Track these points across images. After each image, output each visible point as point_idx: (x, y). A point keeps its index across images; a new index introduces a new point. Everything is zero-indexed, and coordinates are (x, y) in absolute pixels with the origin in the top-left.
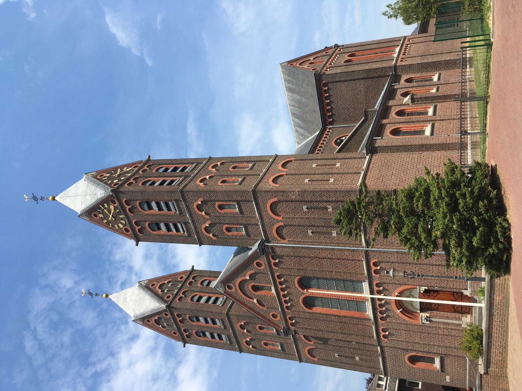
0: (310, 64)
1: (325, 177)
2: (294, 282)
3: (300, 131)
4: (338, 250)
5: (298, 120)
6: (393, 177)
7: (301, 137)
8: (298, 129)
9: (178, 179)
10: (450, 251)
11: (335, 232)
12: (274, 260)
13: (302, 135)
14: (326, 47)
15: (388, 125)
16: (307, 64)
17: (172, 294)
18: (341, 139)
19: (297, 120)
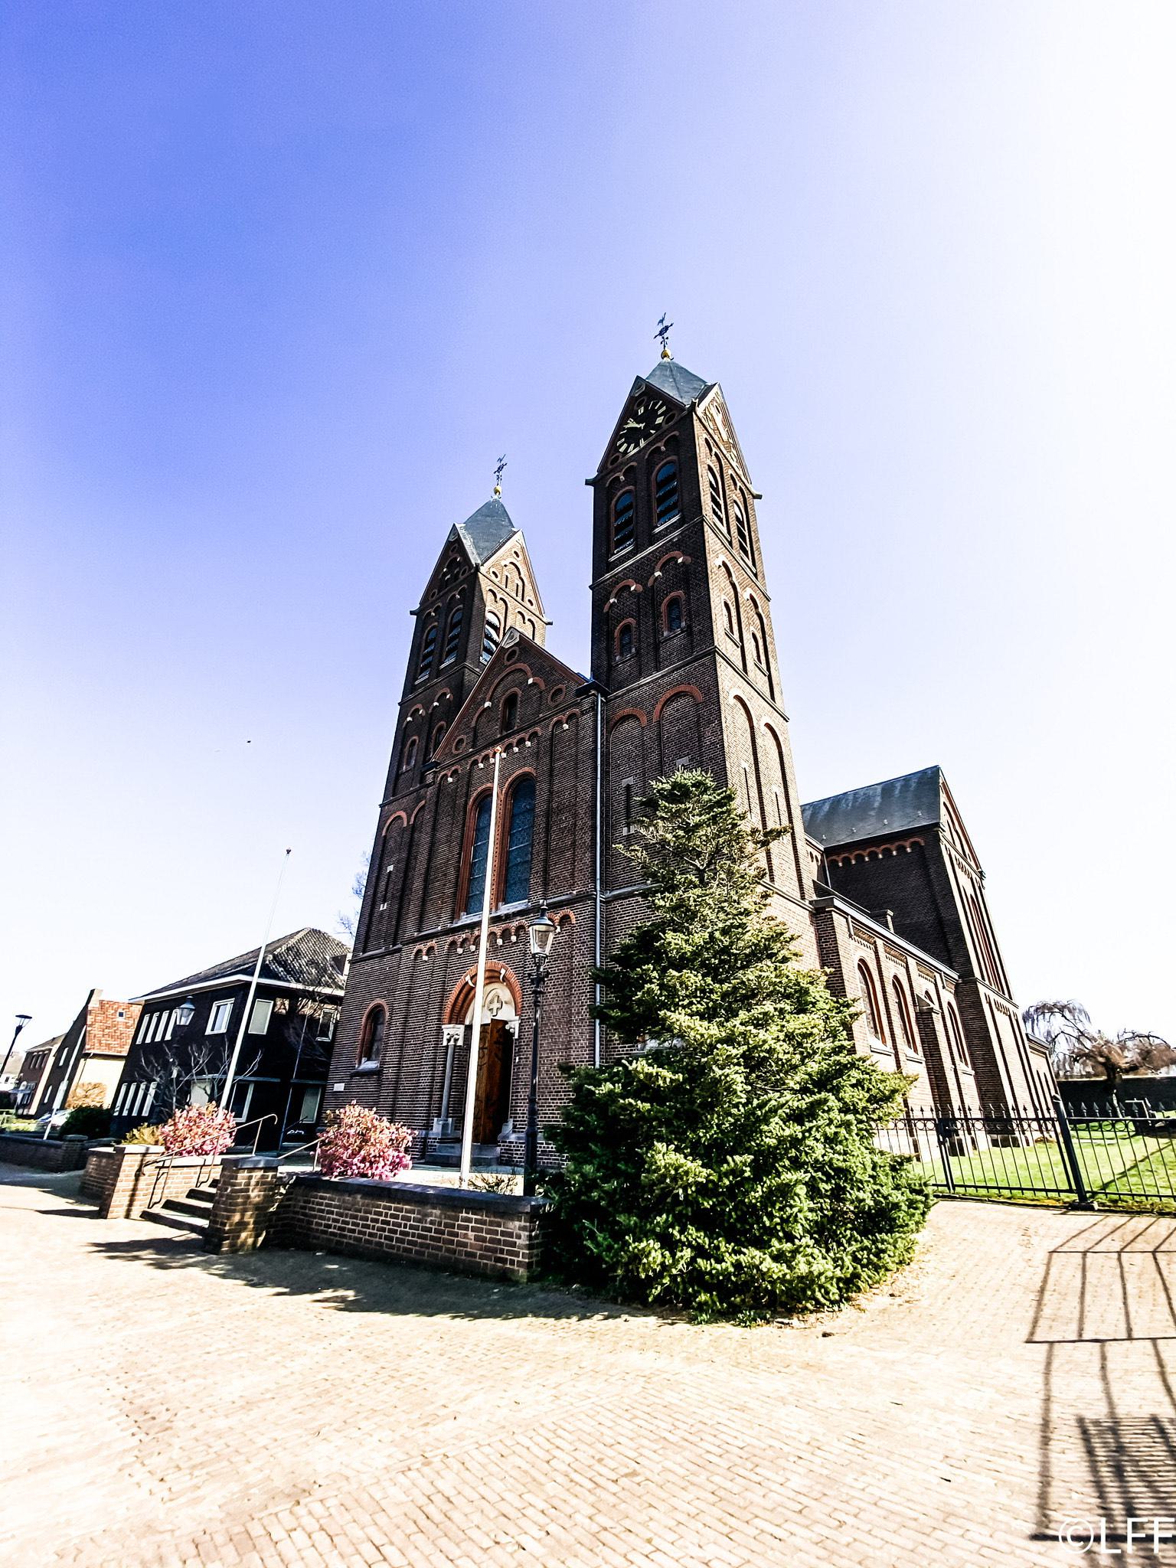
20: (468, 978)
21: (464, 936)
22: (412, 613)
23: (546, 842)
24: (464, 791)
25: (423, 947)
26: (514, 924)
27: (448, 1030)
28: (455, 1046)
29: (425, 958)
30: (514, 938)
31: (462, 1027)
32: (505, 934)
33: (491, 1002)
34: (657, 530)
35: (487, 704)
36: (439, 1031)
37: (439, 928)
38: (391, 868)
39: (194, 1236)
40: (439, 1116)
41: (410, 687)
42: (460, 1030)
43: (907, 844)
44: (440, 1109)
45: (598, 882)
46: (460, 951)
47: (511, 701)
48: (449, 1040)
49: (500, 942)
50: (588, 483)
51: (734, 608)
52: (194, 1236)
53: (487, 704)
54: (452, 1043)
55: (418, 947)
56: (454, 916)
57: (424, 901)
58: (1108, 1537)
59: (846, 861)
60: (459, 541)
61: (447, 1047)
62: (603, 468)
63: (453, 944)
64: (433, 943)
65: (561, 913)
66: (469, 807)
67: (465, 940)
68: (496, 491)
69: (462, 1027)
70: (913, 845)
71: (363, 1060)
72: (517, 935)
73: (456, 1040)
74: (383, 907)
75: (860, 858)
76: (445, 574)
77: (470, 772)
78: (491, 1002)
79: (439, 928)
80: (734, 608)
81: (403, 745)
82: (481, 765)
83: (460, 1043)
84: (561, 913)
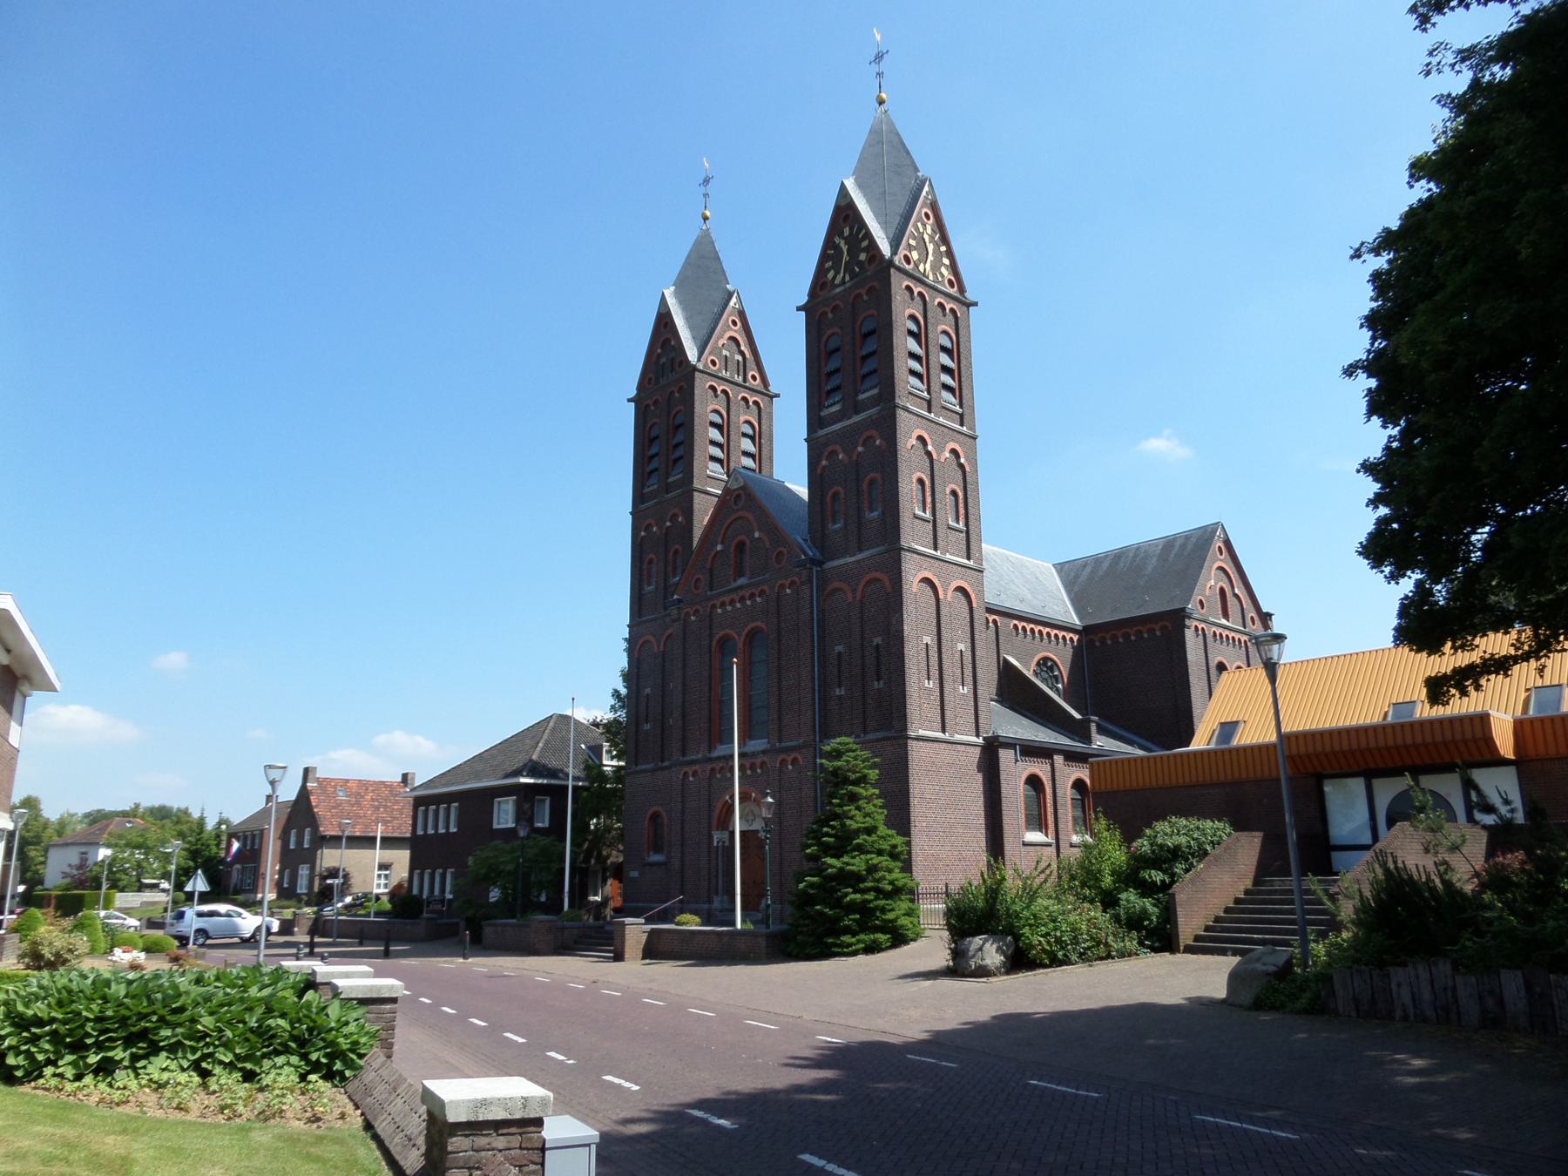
0: (1222, 590)
1: (935, 672)
2: (757, 620)
3: (1084, 573)
4: (814, 699)
5: (1105, 569)
6: (937, 788)
7: (1072, 574)
8: (1088, 569)
9: (924, 387)
10: (1131, 870)
11: (843, 693)
12: (790, 585)
13: (1077, 577)
14: (1269, 615)
15: (1049, 768)
16: (1220, 584)
17: (720, 370)
18: (1055, 668)
19: (1106, 565)
20: (727, 798)
21: (721, 765)
22: (629, 400)
23: (779, 695)
24: (708, 633)
25: (690, 770)
26: (758, 761)
27: (717, 836)
28: (723, 846)
29: (691, 779)
30: (759, 771)
31: (727, 833)
32: (753, 767)
33: (747, 815)
34: (862, 397)
35: (719, 547)
36: (710, 838)
37: (700, 756)
38: (648, 691)
39: (1396, 874)
40: (717, 894)
41: (639, 497)
42: (726, 835)
43: (1157, 627)
44: (717, 890)
45: (817, 735)
46: (718, 776)
47: (741, 547)
48: (718, 842)
49: (749, 772)
50: (799, 309)
51: (929, 488)
52: (1396, 874)
53: (719, 547)
54: (720, 844)
55: (685, 769)
56: (711, 748)
57: (684, 739)
58: (383, 839)
59: (1103, 640)
60: (668, 314)
61: (717, 847)
62: (813, 293)
63: (713, 770)
64: (696, 767)
65: (793, 756)
66: (713, 649)
67: (722, 768)
68: (706, 218)
69: (727, 833)
70: (1163, 628)
71: (651, 853)
72: (761, 768)
73: (724, 842)
74: (647, 727)
75: (1126, 636)
76: (659, 356)
77: (710, 616)
78: (747, 815)
79: (700, 756)
80: (929, 488)
81: (641, 561)
82: (719, 611)
83: (727, 844)
84: (793, 756)
